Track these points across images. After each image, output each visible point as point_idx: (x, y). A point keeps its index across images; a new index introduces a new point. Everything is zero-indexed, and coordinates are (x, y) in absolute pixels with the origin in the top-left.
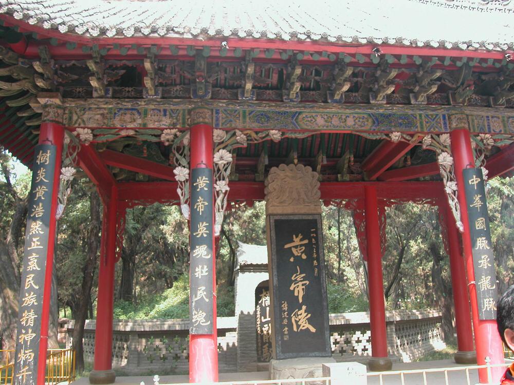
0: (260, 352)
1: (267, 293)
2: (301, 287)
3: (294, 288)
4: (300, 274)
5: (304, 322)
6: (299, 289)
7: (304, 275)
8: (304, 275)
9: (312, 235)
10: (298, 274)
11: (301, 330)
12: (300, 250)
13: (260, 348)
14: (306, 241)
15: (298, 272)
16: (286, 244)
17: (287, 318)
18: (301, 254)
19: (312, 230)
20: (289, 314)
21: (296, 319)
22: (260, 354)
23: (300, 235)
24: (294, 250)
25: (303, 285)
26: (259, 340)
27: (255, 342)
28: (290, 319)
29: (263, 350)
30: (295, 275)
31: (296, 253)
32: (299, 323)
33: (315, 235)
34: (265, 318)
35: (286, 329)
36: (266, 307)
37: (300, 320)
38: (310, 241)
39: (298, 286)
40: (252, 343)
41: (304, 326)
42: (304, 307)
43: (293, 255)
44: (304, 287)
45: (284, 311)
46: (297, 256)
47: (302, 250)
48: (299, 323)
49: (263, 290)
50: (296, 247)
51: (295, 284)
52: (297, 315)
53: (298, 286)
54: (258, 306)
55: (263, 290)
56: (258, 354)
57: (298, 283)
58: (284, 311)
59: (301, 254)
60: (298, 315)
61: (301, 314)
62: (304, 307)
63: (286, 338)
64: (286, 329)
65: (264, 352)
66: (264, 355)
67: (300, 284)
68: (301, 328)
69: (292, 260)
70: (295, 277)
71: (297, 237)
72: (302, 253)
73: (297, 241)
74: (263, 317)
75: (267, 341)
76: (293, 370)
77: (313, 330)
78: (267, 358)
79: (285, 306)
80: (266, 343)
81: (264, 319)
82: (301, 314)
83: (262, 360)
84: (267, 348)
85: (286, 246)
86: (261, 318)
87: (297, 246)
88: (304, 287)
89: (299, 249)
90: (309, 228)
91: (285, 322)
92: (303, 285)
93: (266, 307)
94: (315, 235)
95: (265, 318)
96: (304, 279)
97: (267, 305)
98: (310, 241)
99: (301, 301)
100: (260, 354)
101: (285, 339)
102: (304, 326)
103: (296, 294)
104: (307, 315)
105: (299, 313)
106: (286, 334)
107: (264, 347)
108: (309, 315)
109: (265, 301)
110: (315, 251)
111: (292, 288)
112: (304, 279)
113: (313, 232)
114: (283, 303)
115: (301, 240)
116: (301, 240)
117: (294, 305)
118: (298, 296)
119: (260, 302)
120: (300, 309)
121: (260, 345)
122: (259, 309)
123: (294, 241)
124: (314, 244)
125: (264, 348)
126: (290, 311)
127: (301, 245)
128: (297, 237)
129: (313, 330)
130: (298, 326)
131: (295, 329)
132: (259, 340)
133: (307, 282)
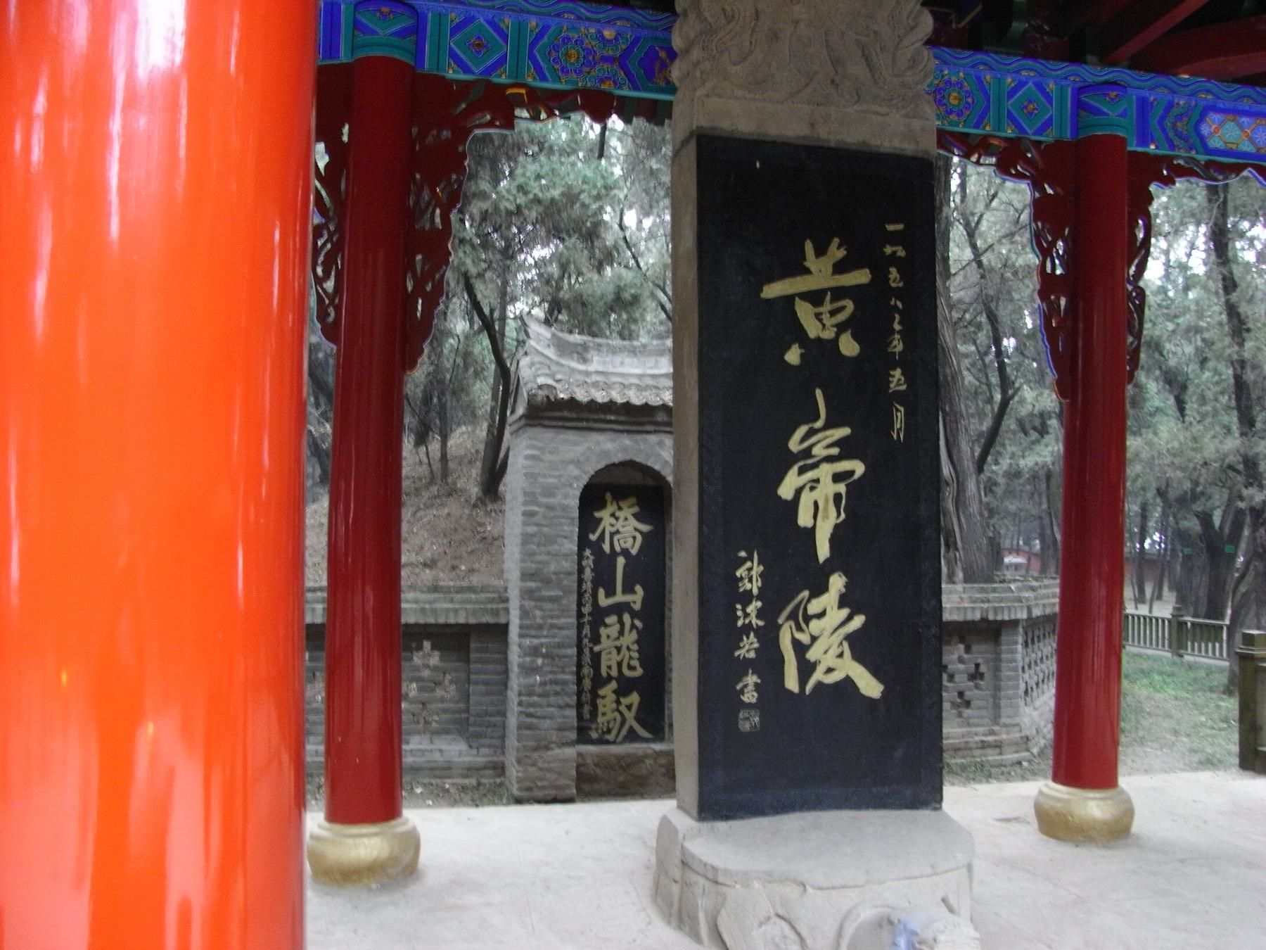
0: (587, 708)
1: (620, 508)
2: (828, 489)
3: (798, 492)
4: (825, 428)
5: (835, 651)
6: (816, 496)
7: (844, 431)
8: (844, 431)
9: (888, 250)
10: (819, 424)
11: (820, 685)
12: (833, 313)
13: (586, 697)
14: (861, 277)
15: (817, 417)
16: (771, 280)
17: (759, 632)
18: (838, 335)
19: (891, 228)
20: (769, 614)
21: (799, 636)
22: (587, 716)
23: (836, 241)
24: (804, 311)
25: (837, 478)
26: (587, 671)
27: (571, 678)
28: (769, 637)
29: (599, 701)
30: (802, 430)
31: (813, 329)
32: (812, 655)
33: (901, 253)
34: (610, 592)
35: (752, 679)
36: (614, 554)
37: (814, 639)
38: (880, 276)
39: (817, 481)
40: (565, 683)
41: (830, 670)
42: (837, 583)
43: (798, 334)
44: (841, 488)
45: (747, 598)
46: (819, 339)
47: (841, 317)
48: (812, 655)
49: (608, 496)
50: (815, 298)
51: (802, 471)
52: (802, 619)
53: (817, 481)
54: (588, 552)
55: (608, 496)
56: (580, 716)
57: (815, 466)
58: (747, 598)
59: (838, 335)
60: (808, 618)
61: (822, 615)
62: (837, 583)
63: (749, 722)
64: (752, 679)
65: (601, 709)
66: (600, 719)
67: (825, 471)
68: (818, 676)
69: (793, 356)
70: (803, 440)
71: (821, 251)
72: (841, 328)
73: (820, 271)
74: (601, 592)
75: (614, 673)
76: (792, 891)
77: (870, 687)
78: (609, 731)
79: (751, 575)
80: (610, 678)
81: (608, 595)
82: (822, 615)
83: (594, 735)
84: (614, 697)
85: (773, 290)
86: (595, 595)
87: (816, 292)
88: (841, 488)
89: (827, 307)
90: (887, 207)
91: (748, 647)
92: (837, 478)
93: (614, 554)
94: (901, 253)
95: (610, 592)
96: (846, 449)
97: (618, 549)
98: (880, 276)
99: (823, 551)
100: (587, 716)
101: (745, 726)
102: (830, 670)
103: (804, 519)
104: (849, 618)
105: (814, 607)
106: (750, 706)
107: (601, 692)
108: (858, 621)
109: (612, 535)
110: (897, 327)
111: (786, 490)
112: (846, 449)
113: (894, 238)
114: (744, 561)
115: (840, 268)
116: (840, 268)
117: (795, 572)
118: (811, 532)
119: (593, 537)
120: (820, 589)
121: (587, 684)
122: (589, 562)
123: (807, 271)
124: (898, 293)
125: (603, 697)
126: (777, 597)
127: (839, 293)
128: (821, 251)
129: (870, 687)
130: (806, 668)
131: (791, 682)
132: (587, 671)
133: (858, 468)
